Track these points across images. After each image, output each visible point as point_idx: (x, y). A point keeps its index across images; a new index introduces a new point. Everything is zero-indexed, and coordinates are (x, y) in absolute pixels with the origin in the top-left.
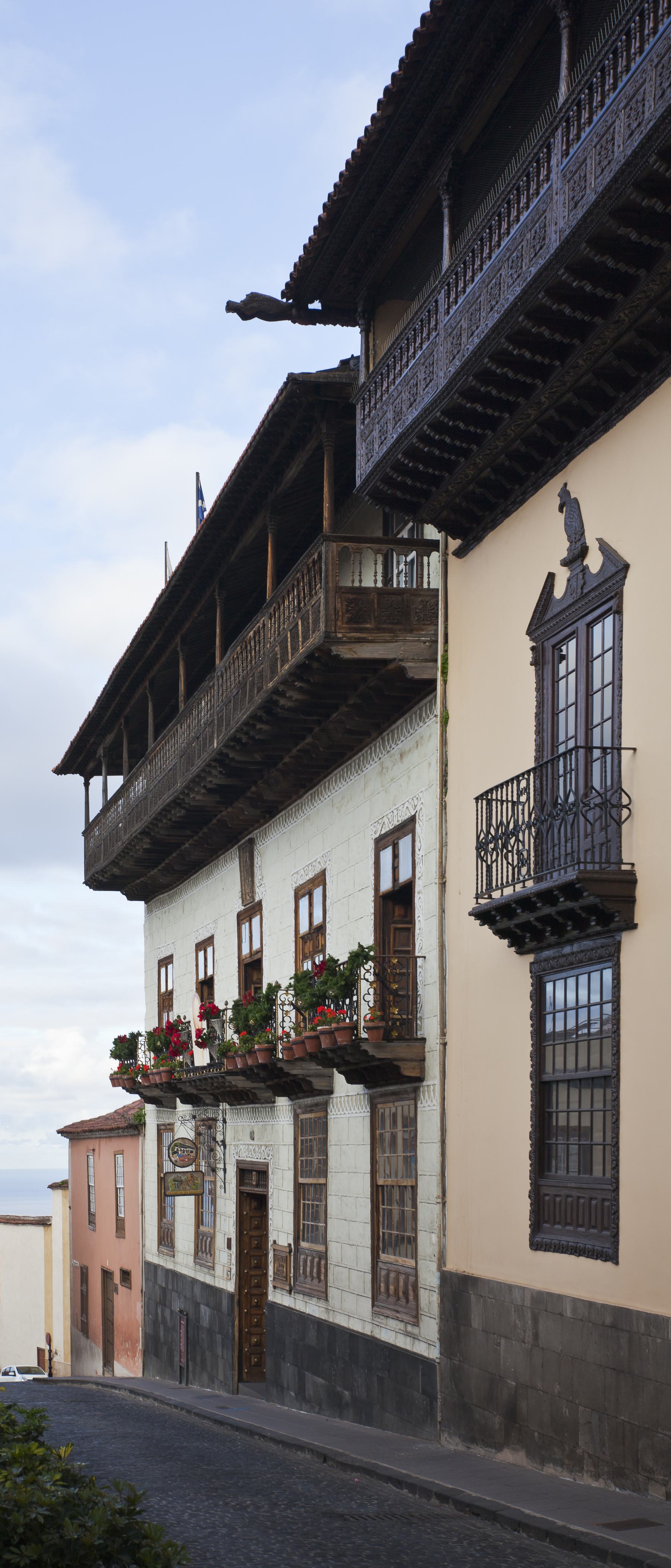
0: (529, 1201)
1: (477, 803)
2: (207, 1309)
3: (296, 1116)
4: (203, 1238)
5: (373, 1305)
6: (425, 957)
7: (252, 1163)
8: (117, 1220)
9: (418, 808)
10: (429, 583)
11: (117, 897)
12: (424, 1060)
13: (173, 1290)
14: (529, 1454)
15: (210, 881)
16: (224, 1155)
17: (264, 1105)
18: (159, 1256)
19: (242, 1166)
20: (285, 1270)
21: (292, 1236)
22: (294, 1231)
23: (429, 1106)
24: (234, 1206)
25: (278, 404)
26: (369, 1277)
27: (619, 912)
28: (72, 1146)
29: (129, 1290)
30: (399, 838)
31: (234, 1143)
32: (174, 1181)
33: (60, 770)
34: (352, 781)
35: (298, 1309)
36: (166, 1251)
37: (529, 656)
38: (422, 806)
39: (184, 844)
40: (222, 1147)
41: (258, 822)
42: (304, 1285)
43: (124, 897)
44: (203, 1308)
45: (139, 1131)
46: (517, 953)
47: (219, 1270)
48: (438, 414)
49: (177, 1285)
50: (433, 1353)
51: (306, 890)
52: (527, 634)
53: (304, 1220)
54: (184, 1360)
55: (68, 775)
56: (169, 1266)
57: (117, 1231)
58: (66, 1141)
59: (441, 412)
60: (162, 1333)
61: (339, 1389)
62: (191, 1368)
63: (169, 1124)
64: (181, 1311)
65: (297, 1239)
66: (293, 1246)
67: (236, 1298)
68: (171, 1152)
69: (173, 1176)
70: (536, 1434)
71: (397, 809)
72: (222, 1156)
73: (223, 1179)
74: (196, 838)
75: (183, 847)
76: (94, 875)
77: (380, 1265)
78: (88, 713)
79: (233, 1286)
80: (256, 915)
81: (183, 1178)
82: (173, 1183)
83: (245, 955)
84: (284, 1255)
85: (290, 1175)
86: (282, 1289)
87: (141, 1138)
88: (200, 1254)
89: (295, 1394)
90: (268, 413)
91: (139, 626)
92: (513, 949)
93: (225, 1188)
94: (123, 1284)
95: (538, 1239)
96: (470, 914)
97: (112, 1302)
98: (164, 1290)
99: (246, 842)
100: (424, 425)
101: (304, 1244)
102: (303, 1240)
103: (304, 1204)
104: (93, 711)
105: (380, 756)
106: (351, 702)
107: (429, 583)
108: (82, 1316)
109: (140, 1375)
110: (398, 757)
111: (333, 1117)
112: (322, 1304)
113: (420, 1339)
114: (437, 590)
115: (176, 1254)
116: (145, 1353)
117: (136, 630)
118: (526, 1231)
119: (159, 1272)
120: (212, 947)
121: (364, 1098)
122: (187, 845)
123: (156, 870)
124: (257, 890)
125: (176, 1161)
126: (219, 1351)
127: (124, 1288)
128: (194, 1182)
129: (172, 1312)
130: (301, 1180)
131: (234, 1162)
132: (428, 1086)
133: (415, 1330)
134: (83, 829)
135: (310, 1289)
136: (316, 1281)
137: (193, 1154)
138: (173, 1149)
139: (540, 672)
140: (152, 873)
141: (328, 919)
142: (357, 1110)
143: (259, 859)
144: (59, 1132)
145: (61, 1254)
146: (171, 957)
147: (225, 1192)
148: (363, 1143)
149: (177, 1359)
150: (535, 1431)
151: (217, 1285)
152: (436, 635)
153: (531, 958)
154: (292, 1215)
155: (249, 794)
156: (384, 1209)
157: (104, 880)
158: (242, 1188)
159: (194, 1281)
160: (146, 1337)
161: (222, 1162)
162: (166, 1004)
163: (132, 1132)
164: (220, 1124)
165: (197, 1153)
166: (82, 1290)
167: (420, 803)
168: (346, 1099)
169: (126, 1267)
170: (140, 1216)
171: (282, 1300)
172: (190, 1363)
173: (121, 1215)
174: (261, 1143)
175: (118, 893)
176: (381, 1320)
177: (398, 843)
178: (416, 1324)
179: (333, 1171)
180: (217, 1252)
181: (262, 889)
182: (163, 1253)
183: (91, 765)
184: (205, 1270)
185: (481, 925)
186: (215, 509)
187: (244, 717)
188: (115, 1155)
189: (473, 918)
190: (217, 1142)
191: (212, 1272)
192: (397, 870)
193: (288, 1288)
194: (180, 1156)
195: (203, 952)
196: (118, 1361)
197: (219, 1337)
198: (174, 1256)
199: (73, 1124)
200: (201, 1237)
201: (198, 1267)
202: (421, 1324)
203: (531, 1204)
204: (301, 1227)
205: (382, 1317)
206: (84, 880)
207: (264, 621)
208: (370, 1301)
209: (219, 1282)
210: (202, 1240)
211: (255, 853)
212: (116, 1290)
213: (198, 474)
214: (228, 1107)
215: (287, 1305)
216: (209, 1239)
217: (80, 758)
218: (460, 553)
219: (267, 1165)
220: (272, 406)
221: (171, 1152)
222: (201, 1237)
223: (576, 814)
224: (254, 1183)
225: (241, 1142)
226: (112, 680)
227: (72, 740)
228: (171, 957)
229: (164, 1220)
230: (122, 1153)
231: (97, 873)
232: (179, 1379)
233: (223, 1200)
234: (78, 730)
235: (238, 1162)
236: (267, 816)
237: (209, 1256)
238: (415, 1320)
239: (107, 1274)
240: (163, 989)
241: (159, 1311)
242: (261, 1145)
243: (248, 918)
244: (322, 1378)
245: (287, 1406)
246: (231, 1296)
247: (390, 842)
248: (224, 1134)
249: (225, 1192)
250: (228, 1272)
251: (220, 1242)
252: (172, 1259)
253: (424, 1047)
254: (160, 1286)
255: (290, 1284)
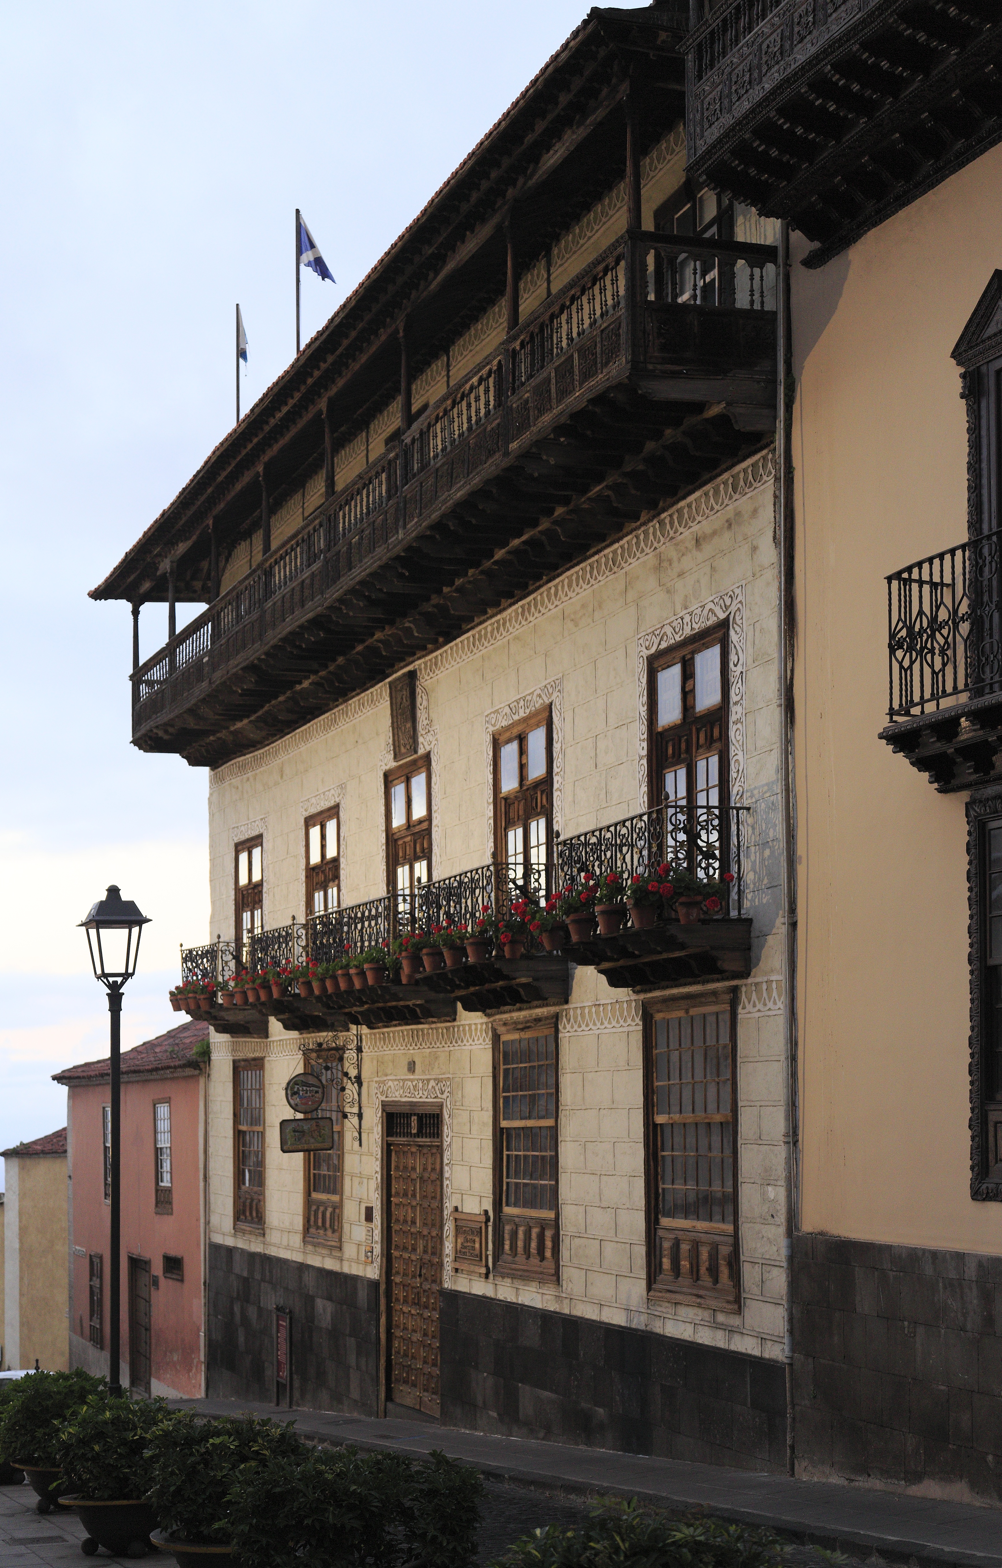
0: (969, 1133)
1: (889, 583)
2: (328, 1304)
3: (496, 1038)
4: (318, 1209)
5: (649, 1288)
6: (748, 809)
7: (412, 1104)
8: (157, 1191)
9: (733, 609)
10: (762, 303)
11: (175, 761)
12: (749, 949)
13: (263, 1280)
14: (974, 1485)
15: (331, 734)
16: (359, 1094)
17: (433, 1026)
18: (235, 1236)
19: (389, 1109)
20: (477, 1245)
21: (491, 1200)
22: (494, 1193)
23: (759, 1011)
24: (379, 1163)
25: (566, 52)
26: (641, 1251)
27: (181, 945)
28: (72, 1097)
29: (178, 1284)
30: (693, 653)
31: (377, 1079)
32: (294, 1131)
33: (99, 594)
34: (602, 583)
35: (501, 1298)
36: (248, 1229)
37: (958, 385)
38: (739, 605)
39: (300, 683)
40: (356, 1085)
41: (424, 648)
42: (514, 1266)
43: (185, 761)
44: (320, 1303)
45: (201, 1069)
46: (940, 791)
47: (350, 1250)
48: (856, 47)
49: (271, 1272)
50: (777, 1352)
51: (515, 731)
52: (953, 355)
53: (508, 1177)
54: (285, 1373)
55: (109, 601)
56: (256, 1247)
57: (157, 1206)
58: (63, 1090)
59: (861, 44)
60: (241, 1339)
61: (584, 1405)
62: (296, 1384)
63: (254, 1059)
64: (278, 1309)
65: (498, 1204)
66: (491, 1214)
67: (383, 1287)
68: (289, 1092)
69: (293, 1125)
70: (990, 1458)
71: (691, 614)
72: (356, 1096)
73: (357, 1127)
74: (323, 673)
75: (298, 687)
76: (151, 731)
77: (660, 1233)
78: (161, 512)
79: (377, 1272)
80: (420, 773)
81: (305, 1128)
82: (292, 1134)
83: (398, 828)
84: (478, 1226)
85: (487, 1116)
86: (470, 1273)
87: (202, 1081)
88: (312, 1230)
89: (498, 1414)
90: (547, 66)
91: (270, 384)
92: (936, 785)
93: (360, 1140)
94: (168, 1275)
95: (987, 1185)
96: (881, 737)
97: (148, 1301)
98: (246, 1282)
99: (404, 675)
100: (826, 64)
101: (508, 1210)
102: (507, 1205)
103: (508, 1156)
104: (169, 508)
105: (655, 544)
106: (628, 468)
107: (762, 303)
108: (91, 1320)
109: (201, 1394)
110: (691, 544)
111: (568, 1035)
112: (550, 1291)
113: (745, 1331)
114: (775, 313)
115: (267, 1231)
116: (210, 1365)
117: (265, 390)
118: (966, 1176)
119: (237, 1257)
120: (334, 821)
121: (629, 1006)
122: (306, 684)
123: (246, 721)
124: (421, 740)
125: (296, 1105)
126: (352, 1360)
127: (170, 1282)
128: (319, 1132)
129: (260, 1309)
130: (504, 1124)
131: (377, 1104)
132: (756, 984)
133: (735, 1321)
134: (131, 672)
135: (524, 1271)
136: (534, 1260)
137: (319, 1095)
138: (292, 1089)
139: (975, 407)
140: (239, 725)
141: (556, 770)
142: (614, 1023)
143: (424, 697)
144: (54, 1078)
145: (17, 1240)
146: (260, 836)
147: (360, 1145)
148: (627, 1068)
149: (269, 1372)
150: (987, 1454)
151: (346, 1270)
152: (775, 372)
153: (964, 796)
154: (490, 1172)
155: (427, 607)
156: (314, 1174)
157: (166, 737)
158: (389, 1139)
159: (302, 1267)
160: (211, 1345)
161: (357, 1105)
162: (257, 899)
163: (189, 1071)
164: (350, 1055)
165: (323, 1093)
166: (91, 1287)
167: (735, 602)
168: (594, 1010)
169: (172, 1253)
170: (202, 1184)
171: (471, 1287)
172: (295, 1377)
173: (166, 1183)
174: (428, 1077)
175: (177, 756)
176: (665, 1309)
177: (693, 659)
178: (739, 1311)
179: (567, 1108)
180: (346, 1227)
181: (429, 737)
182: (244, 1232)
183: (146, 586)
184: (325, 1251)
185: (894, 752)
186: (430, 210)
187: (459, 495)
188: (155, 1105)
189: (884, 741)
190: (350, 1078)
191: (336, 1253)
192: (689, 697)
193: (483, 1270)
194: (301, 1098)
195: (318, 828)
196: (159, 1379)
197: (351, 1342)
198: (264, 1235)
199: (75, 1067)
200: (314, 1208)
201: (310, 1247)
202: (747, 1313)
203: (973, 1138)
204: (505, 1188)
205: (667, 1304)
206: (131, 739)
207: (500, 361)
208: (643, 1284)
209: (350, 1266)
210: (316, 1212)
211: (418, 690)
212: (155, 1282)
213: (298, 211)
214: (365, 1030)
215: (481, 1294)
216: (330, 1210)
217: (132, 577)
218: (813, 261)
219: (441, 1106)
220: (555, 58)
221: (289, 1092)
222: (314, 1208)
223: (934, 619)
224: (414, 1131)
225: (389, 1078)
226: (210, 464)
227: (128, 550)
228: (260, 836)
229: (243, 1187)
230: (168, 1100)
231: (157, 727)
232: (275, 1399)
233: (356, 1158)
234: (140, 535)
235: (384, 1105)
236: (441, 640)
237: (329, 1232)
238: (736, 1307)
239: (138, 1265)
240: (243, 880)
241: (237, 1309)
242: (428, 1080)
243: (403, 778)
244: (551, 1391)
245: (483, 1431)
246: (374, 1285)
247: (677, 660)
248: (359, 1067)
249: (360, 1145)
250: (366, 1253)
251: (352, 1212)
252: (261, 1238)
253: (750, 932)
254: (239, 1277)
255: (487, 1266)
